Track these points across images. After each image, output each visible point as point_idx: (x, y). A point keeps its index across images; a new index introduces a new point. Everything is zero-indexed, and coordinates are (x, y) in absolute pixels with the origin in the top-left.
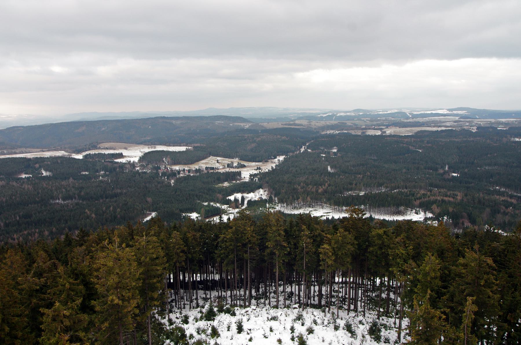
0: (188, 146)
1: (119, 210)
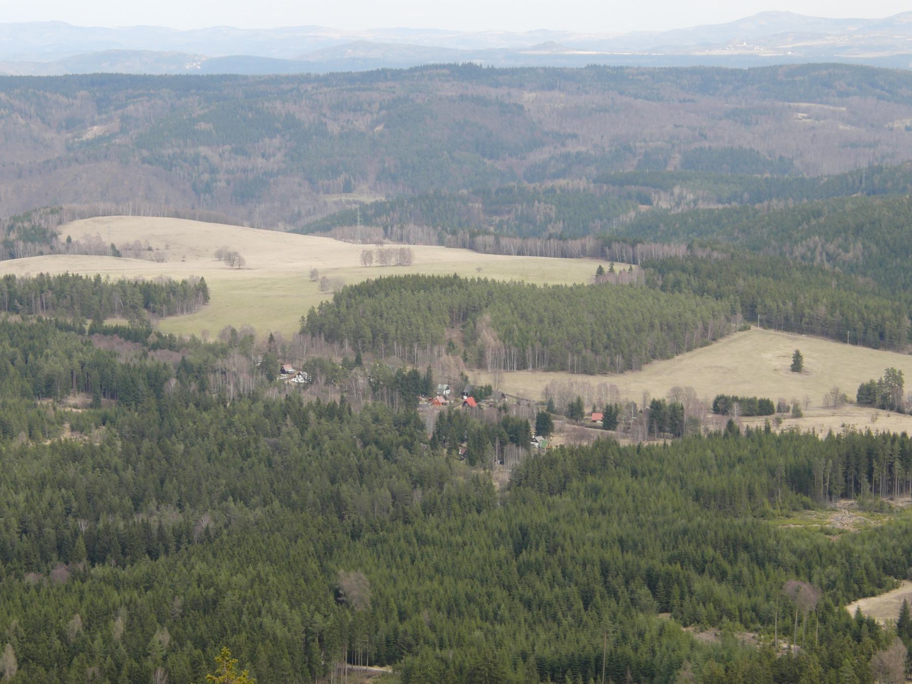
0: (613, 259)
1: (162, 637)
